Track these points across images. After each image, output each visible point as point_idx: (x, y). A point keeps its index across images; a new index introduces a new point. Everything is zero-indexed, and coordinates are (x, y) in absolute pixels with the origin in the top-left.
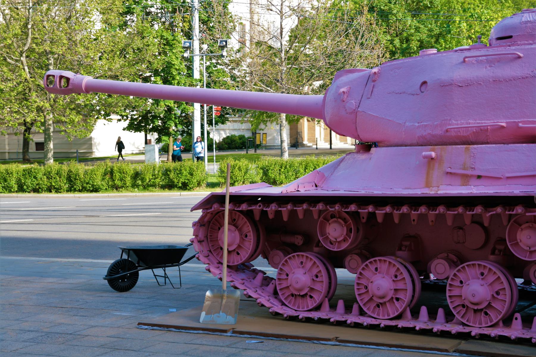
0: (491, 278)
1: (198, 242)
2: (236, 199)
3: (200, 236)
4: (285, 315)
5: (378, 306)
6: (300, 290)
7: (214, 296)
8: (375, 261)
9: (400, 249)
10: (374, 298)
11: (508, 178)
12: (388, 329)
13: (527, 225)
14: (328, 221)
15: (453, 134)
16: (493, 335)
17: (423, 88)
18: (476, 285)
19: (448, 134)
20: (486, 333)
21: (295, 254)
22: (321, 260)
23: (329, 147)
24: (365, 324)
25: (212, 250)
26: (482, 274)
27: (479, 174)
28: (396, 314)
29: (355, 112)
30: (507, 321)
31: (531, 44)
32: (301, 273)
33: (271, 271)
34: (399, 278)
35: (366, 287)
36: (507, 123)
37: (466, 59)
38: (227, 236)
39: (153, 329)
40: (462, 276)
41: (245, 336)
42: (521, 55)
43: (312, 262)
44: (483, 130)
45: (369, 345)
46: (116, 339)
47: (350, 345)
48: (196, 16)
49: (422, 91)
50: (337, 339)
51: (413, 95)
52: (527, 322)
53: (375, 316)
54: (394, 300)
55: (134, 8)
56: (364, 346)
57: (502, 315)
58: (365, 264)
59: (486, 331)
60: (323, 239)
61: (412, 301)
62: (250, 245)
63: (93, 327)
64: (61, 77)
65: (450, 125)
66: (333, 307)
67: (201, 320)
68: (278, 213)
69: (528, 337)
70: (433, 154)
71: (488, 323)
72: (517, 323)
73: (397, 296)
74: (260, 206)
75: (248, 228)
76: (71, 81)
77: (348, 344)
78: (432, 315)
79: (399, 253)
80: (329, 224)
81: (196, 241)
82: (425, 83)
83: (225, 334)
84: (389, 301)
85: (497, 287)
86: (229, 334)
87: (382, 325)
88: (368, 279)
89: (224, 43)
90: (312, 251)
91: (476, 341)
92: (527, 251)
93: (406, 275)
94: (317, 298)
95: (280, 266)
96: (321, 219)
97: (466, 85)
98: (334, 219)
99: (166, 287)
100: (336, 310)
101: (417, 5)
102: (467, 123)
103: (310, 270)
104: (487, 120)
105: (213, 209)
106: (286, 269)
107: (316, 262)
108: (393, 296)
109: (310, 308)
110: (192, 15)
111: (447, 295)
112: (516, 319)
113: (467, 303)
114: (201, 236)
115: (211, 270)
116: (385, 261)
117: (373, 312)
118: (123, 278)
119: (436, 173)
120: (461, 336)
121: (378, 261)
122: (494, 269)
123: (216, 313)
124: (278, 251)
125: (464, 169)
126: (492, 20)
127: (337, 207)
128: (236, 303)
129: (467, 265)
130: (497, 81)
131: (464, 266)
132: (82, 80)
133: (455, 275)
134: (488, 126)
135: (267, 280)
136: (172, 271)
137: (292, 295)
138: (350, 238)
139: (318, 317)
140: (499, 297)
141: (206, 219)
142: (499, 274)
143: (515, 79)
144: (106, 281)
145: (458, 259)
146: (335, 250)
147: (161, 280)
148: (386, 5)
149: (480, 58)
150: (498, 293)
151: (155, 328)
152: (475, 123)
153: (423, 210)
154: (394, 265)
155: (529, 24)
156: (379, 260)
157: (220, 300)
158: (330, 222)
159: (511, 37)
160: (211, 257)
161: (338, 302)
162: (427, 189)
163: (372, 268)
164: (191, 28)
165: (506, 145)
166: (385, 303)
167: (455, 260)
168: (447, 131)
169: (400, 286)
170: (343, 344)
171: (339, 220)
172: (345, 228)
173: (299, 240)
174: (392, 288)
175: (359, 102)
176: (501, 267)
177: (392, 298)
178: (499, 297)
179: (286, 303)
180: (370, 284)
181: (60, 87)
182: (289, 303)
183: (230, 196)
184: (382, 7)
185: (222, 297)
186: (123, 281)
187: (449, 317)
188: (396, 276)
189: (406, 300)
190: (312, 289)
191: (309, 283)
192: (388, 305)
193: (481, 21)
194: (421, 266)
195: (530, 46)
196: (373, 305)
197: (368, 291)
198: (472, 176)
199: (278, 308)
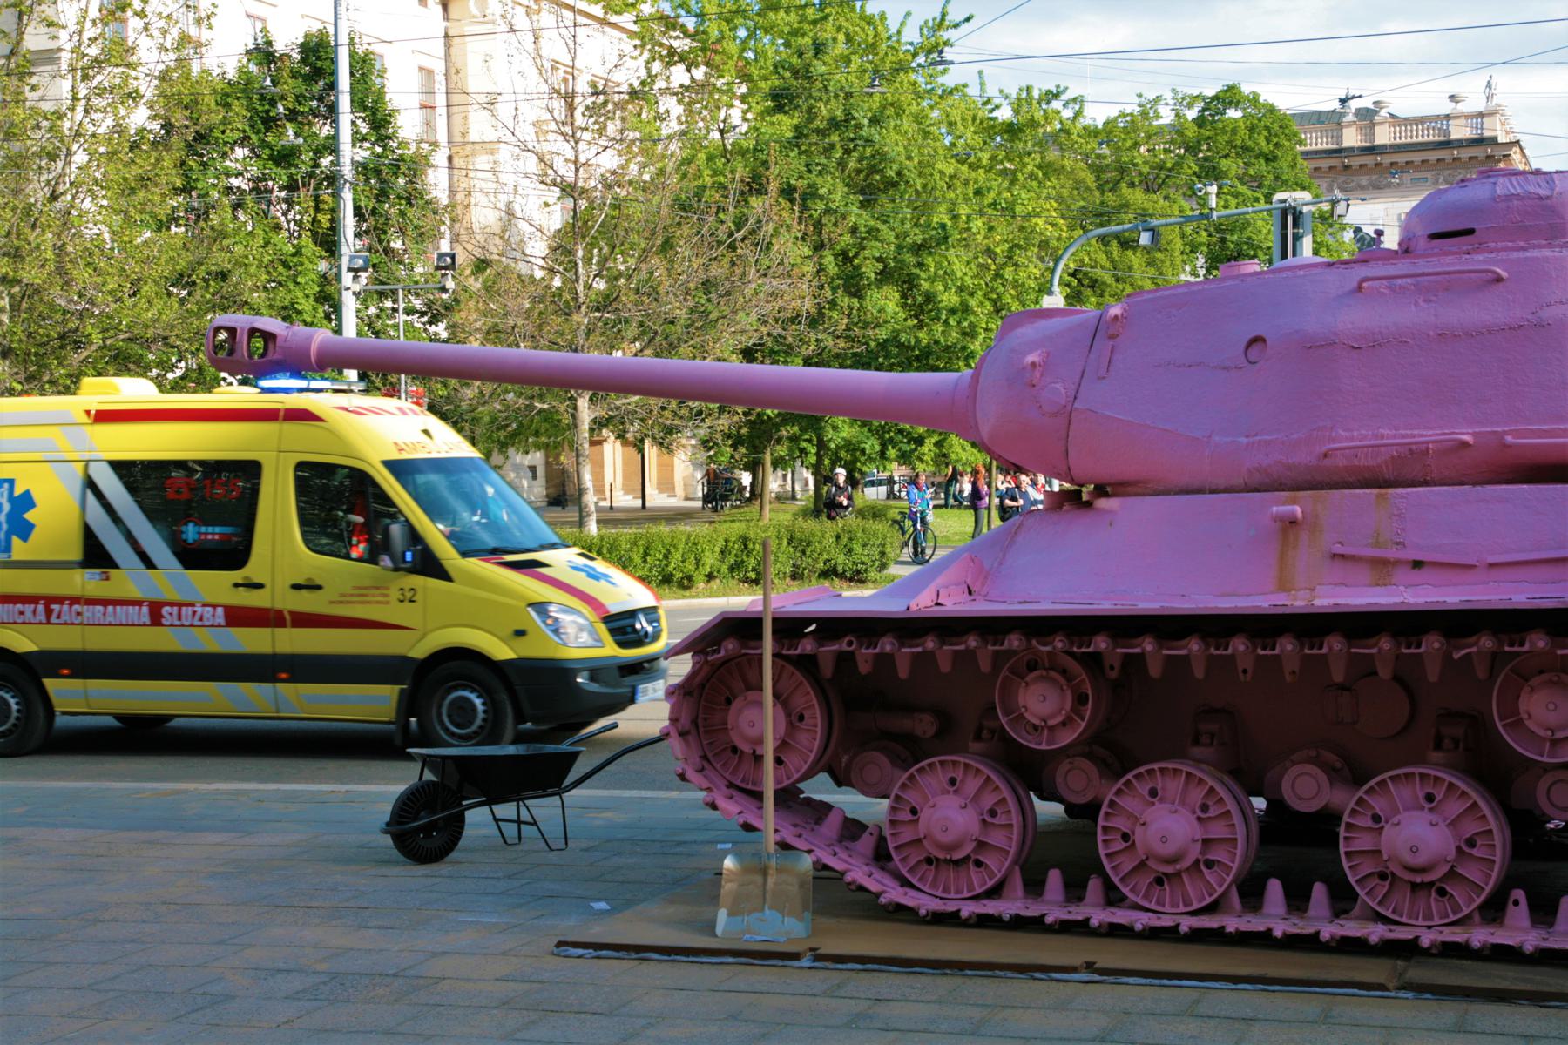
0: (1455, 807)
2: (789, 627)
3: (682, 720)
7: (746, 870)
9: (1196, 742)
11: (1491, 565)
12: (1199, 937)
13: (1545, 677)
14: (1023, 678)
15: (1341, 462)
17: (1255, 349)
18: (1417, 825)
19: (1327, 462)
20: (991, 911)
23: (639, 503)
25: (710, 755)
26: (1430, 798)
29: (1067, 414)
30: (1493, 910)
32: (952, 807)
33: (870, 808)
34: (1213, 812)
36: (1474, 434)
38: (762, 720)
39: (598, 957)
40: (1378, 804)
41: (850, 966)
42: (1504, 274)
43: (980, 781)
44: (1418, 453)
46: (526, 986)
47: (1131, 980)
48: (347, 196)
49: (1252, 359)
50: (1090, 966)
51: (1227, 369)
52: (1543, 912)
53: (1152, 906)
55: (197, 180)
56: (1165, 982)
57: (1483, 896)
58: (1124, 780)
59: (1456, 936)
60: (1010, 722)
62: (811, 740)
63: (434, 955)
64: (253, 332)
65: (1333, 440)
66: (1034, 886)
67: (719, 930)
68: (885, 661)
69: (1080, 918)
71: (1432, 919)
72: (1518, 913)
74: (850, 643)
75: (808, 699)
76: (279, 342)
77: (1125, 979)
78: (1075, 890)
79: (1196, 751)
81: (674, 733)
82: (1257, 340)
83: (796, 963)
85: (1471, 828)
86: (805, 962)
87: (1184, 929)
88: (1130, 816)
89: (449, 260)
91: (1432, 960)
92: (1544, 739)
94: (997, 866)
95: (895, 791)
96: (1004, 672)
97: (1368, 346)
98: (1037, 673)
99: (520, 847)
100: (1041, 895)
101: (867, 176)
102: (1376, 437)
103: (976, 798)
104: (1426, 428)
105: (722, 653)
106: (911, 797)
107: (993, 776)
109: (978, 890)
110: (336, 195)
111: (1342, 849)
112: (1516, 903)
113: (1394, 868)
114: (685, 721)
115: (721, 802)
118: (427, 829)
120: (1391, 949)
123: (755, 910)
124: (875, 754)
125: (1377, 545)
126: (1038, 215)
127: (1059, 643)
128: (802, 885)
130: (1446, 336)
131: (1384, 781)
132: (310, 338)
133: (1360, 801)
135: (852, 829)
136: (544, 808)
137: (929, 861)
139: (1013, 912)
140: (1475, 852)
141: (698, 679)
144: (388, 840)
146: (1044, 747)
147: (510, 830)
148: (801, 177)
149: (1399, 281)
150: (1471, 843)
151: (604, 953)
152: (1394, 437)
153: (1016, 643)
156: (1161, 770)
157: (759, 879)
159: (1471, 232)
160: (709, 771)
161: (1046, 874)
162: (1283, 595)
163: (1143, 789)
164: (334, 228)
165: (1479, 488)
166: (1178, 874)
167: (1338, 765)
168: (1325, 456)
169: (1218, 830)
170: (1111, 979)
171: (1052, 674)
173: (924, 726)
174: (1198, 836)
175: (1074, 387)
177: (1198, 861)
178: (1475, 852)
179: (914, 882)
180: (1139, 830)
181: (250, 356)
183: (774, 620)
184: (793, 182)
185: (764, 872)
186: (428, 836)
187: (1343, 899)
190: (981, 845)
191: (975, 829)
193: (1014, 217)
195: (1521, 254)
196: (1145, 881)
198: (1397, 563)
199: (895, 894)
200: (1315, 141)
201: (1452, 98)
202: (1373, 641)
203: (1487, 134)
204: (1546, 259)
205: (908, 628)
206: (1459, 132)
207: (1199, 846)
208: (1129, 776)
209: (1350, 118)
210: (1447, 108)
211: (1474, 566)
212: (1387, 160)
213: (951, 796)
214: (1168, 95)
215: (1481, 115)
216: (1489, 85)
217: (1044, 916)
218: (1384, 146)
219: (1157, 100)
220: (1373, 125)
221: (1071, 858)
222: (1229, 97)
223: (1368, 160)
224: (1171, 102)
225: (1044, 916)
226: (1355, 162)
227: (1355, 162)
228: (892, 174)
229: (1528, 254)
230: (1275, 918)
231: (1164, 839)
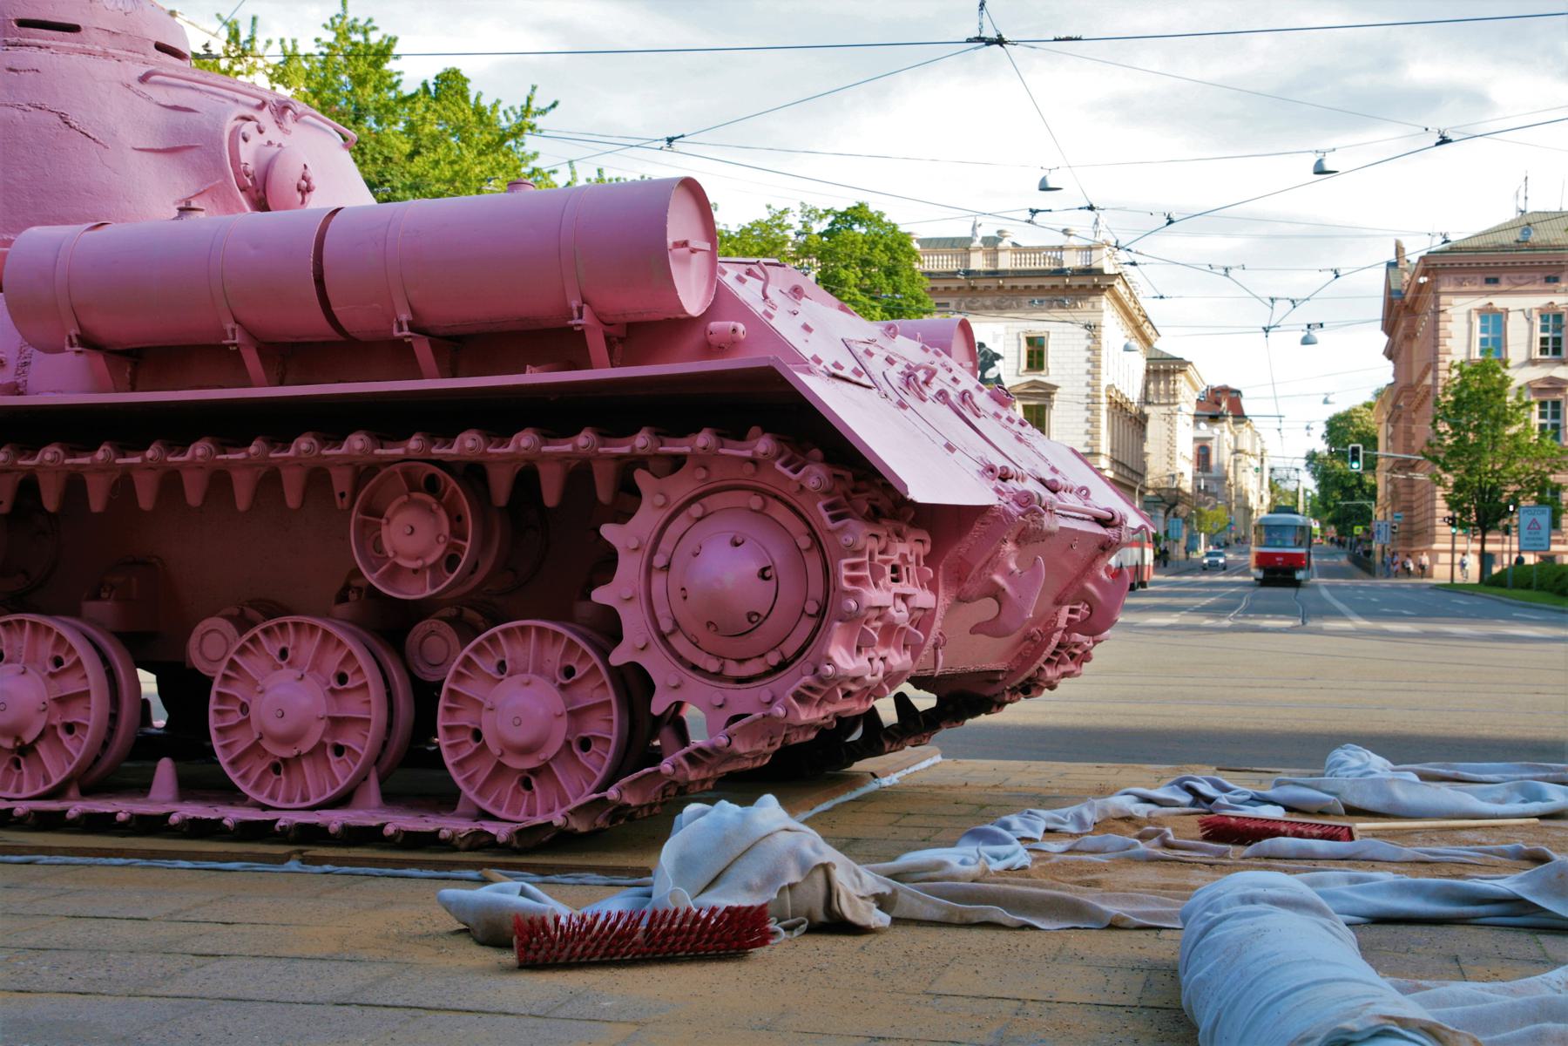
5: (276, 768)
8: (282, 626)
21: (272, 623)
35: (244, 708)
45: (107, 856)
54: (330, 754)
71: (500, 808)
73: (340, 742)
79: (90, 607)
80: (388, 522)
84: (311, 753)
90: (76, 613)
103: (316, 666)
108: (326, 740)
109: (313, 801)
121: (290, 627)
122: (338, 633)
129: (505, 632)
131: (495, 635)
158: (388, 513)
163: (272, 647)
172: (442, 513)
174: (323, 712)
176: (361, 632)
177: (568, 743)
182: (244, 777)
188: (342, 678)
192: (307, 766)
197: (483, 749)
200: (944, 263)
201: (1065, 232)
202: (627, 440)
203: (1095, 265)
206: (1072, 261)
207: (322, 725)
209: (977, 243)
210: (1061, 240)
212: (1008, 284)
213: (507, 680)
214: (797, 208)
215: (1090, 248)
216: (1096, 223)
217: (383, 826)
218: (1006, 271)
219: (785, 211)
220: (996, 251)
221: (413, 769)
222: (857, 214)
223: (992, 283)
224: (799, 215)
225: (383, 826)
226: (981, 284)
227: (981, 284)
228: (262, 81)
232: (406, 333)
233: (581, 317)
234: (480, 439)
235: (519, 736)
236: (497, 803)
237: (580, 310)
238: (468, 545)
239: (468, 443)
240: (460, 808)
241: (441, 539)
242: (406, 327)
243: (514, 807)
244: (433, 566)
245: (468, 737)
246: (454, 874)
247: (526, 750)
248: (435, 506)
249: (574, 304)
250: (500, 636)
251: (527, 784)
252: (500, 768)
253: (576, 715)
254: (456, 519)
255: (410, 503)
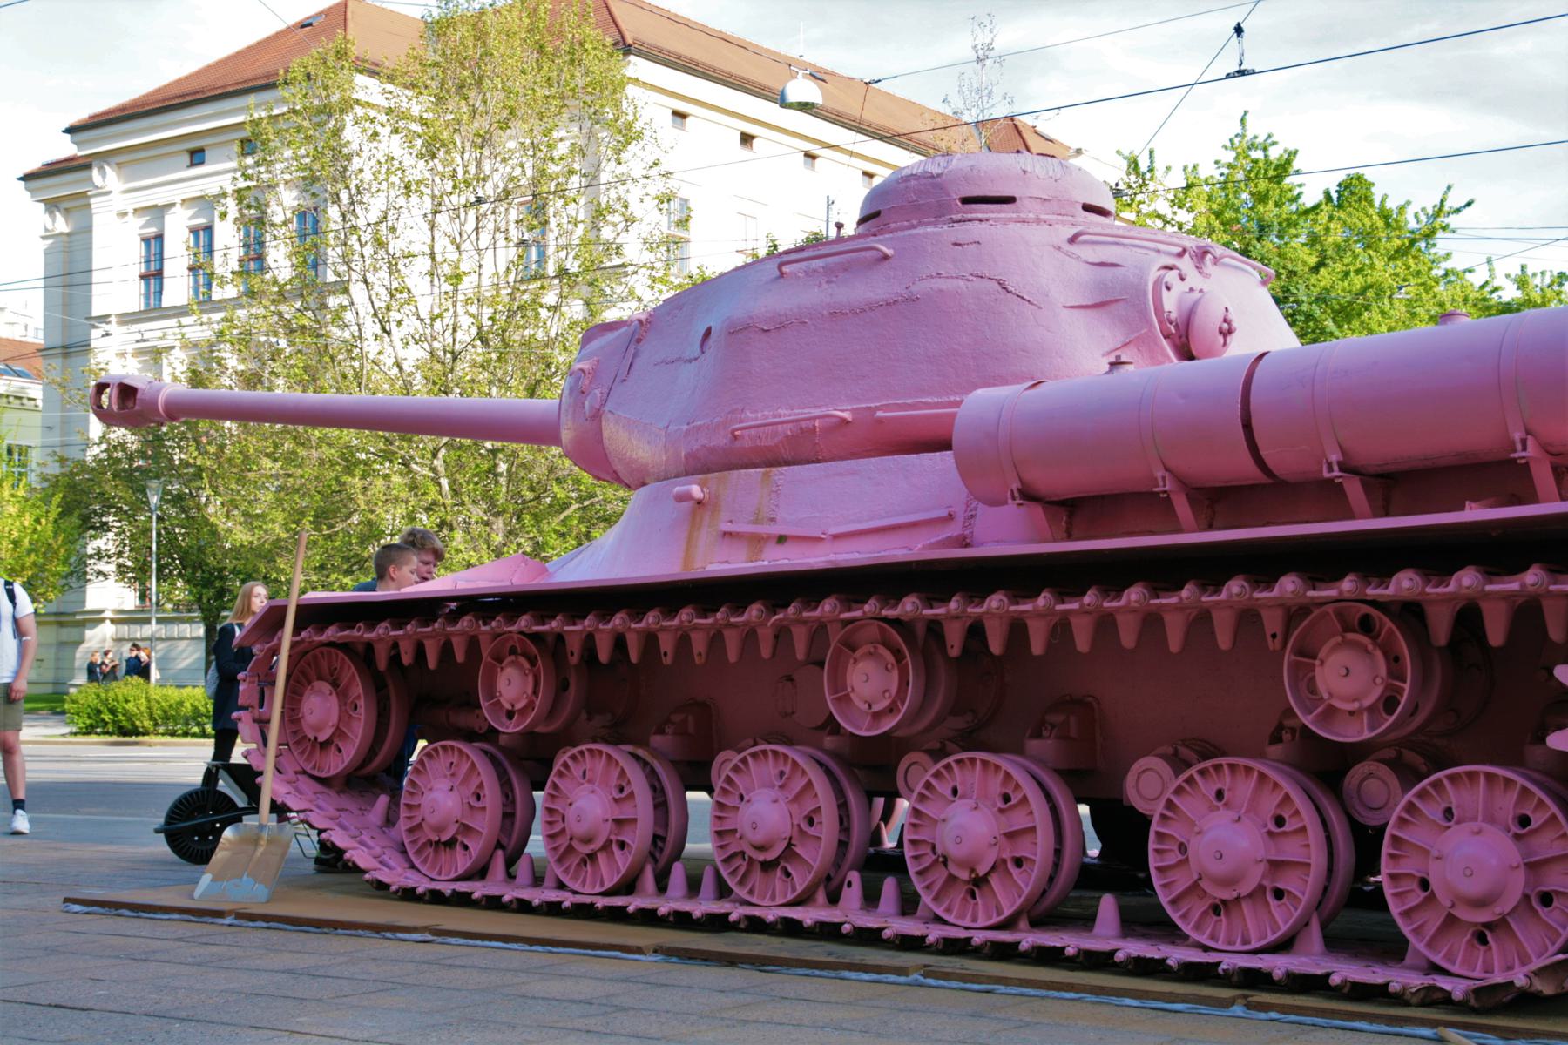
1: (254, 721)
4: (394, 888)
5: (1216, 910)
6: (439, 829)
8: (1218, 768)
10: (575, 844)
11: (836, 537)
15: (747, 443)
16: (663, 911)
19: (738, 444)
22: (821, 764)
24: (536, 902)
27: (783, 533)
28: (1271, 938)
31: (913, 227)
36: (852, 410)
37: (786, 269)
42: (889, 252)
61: (1051, 879)
70: (696, 491)
73: (1280, 886)
83: (220, 921)
84: (1250, 896)
93: (1308, 817)
97: (779, 326)
103: (1253, 808)
112: (850, 884)
116: (1248, 770)
117: (575, 878)
119: (705, 537)
122: (1273, 775)
125: (756, 522)
129: (1451, 778)
130: (836, 314)
134: (814, 418)
138: (903, 703)
142: (1287, 787)
143: (872, 307)
145: (1194, 751)
154: (1276, 785)
155: (913, 183)
163: (1207, 788)
172: (1378, 654)
174: (1261, 854)
177: (1526, 897)
188: (1280, 821)
189: (1304, 899)
194: (1091, 776)
196: (1199, 907)
197: (1432, 897)
198: (768, 538)
204: (926, 235)
205: (472, 604)
208: (950, 760)
211: (819, 539)
213: (1455, 828)
217: (1328, 975)
229: (920, 230)
230: (850, 913)
231: (959, 840)
232: (1336, 473)
233: (1524, 449)
234: (1417, 578)
235: (1472, 888)
236: (1450, 957)
237: (1524, 442)
238: (1407, 686)
239: (1405, 583)
240: (1408, 960)
241: (1378, 681)
242: (1336, 468)
243: (1469, 962)
244: (1371, 709)
245: (1415, 885)
246: (1407, 1030)
247: (1480, 903)
248: (1370, 647)
249: (1517, 436)
250: (1445, 782)
251: (1482, 939)
252: (1451, 921)
253: (1533, 867)
254: (1394, 660)
255: (1346, 644)
